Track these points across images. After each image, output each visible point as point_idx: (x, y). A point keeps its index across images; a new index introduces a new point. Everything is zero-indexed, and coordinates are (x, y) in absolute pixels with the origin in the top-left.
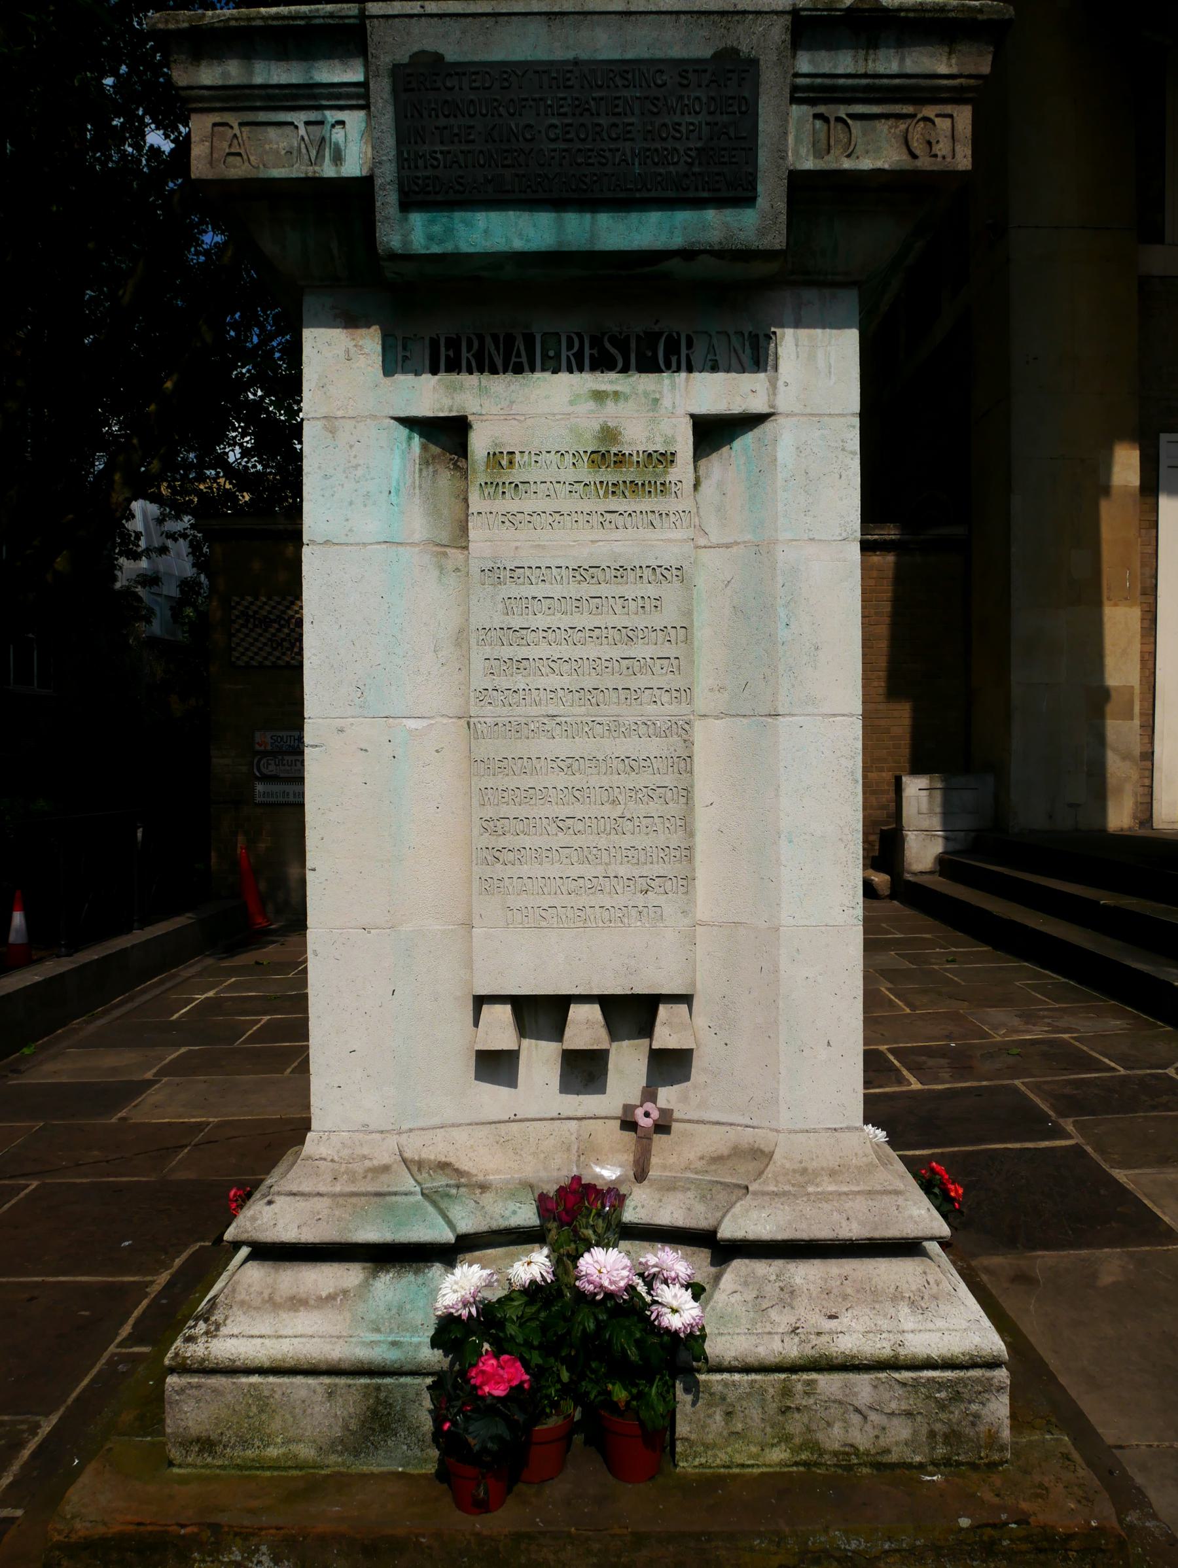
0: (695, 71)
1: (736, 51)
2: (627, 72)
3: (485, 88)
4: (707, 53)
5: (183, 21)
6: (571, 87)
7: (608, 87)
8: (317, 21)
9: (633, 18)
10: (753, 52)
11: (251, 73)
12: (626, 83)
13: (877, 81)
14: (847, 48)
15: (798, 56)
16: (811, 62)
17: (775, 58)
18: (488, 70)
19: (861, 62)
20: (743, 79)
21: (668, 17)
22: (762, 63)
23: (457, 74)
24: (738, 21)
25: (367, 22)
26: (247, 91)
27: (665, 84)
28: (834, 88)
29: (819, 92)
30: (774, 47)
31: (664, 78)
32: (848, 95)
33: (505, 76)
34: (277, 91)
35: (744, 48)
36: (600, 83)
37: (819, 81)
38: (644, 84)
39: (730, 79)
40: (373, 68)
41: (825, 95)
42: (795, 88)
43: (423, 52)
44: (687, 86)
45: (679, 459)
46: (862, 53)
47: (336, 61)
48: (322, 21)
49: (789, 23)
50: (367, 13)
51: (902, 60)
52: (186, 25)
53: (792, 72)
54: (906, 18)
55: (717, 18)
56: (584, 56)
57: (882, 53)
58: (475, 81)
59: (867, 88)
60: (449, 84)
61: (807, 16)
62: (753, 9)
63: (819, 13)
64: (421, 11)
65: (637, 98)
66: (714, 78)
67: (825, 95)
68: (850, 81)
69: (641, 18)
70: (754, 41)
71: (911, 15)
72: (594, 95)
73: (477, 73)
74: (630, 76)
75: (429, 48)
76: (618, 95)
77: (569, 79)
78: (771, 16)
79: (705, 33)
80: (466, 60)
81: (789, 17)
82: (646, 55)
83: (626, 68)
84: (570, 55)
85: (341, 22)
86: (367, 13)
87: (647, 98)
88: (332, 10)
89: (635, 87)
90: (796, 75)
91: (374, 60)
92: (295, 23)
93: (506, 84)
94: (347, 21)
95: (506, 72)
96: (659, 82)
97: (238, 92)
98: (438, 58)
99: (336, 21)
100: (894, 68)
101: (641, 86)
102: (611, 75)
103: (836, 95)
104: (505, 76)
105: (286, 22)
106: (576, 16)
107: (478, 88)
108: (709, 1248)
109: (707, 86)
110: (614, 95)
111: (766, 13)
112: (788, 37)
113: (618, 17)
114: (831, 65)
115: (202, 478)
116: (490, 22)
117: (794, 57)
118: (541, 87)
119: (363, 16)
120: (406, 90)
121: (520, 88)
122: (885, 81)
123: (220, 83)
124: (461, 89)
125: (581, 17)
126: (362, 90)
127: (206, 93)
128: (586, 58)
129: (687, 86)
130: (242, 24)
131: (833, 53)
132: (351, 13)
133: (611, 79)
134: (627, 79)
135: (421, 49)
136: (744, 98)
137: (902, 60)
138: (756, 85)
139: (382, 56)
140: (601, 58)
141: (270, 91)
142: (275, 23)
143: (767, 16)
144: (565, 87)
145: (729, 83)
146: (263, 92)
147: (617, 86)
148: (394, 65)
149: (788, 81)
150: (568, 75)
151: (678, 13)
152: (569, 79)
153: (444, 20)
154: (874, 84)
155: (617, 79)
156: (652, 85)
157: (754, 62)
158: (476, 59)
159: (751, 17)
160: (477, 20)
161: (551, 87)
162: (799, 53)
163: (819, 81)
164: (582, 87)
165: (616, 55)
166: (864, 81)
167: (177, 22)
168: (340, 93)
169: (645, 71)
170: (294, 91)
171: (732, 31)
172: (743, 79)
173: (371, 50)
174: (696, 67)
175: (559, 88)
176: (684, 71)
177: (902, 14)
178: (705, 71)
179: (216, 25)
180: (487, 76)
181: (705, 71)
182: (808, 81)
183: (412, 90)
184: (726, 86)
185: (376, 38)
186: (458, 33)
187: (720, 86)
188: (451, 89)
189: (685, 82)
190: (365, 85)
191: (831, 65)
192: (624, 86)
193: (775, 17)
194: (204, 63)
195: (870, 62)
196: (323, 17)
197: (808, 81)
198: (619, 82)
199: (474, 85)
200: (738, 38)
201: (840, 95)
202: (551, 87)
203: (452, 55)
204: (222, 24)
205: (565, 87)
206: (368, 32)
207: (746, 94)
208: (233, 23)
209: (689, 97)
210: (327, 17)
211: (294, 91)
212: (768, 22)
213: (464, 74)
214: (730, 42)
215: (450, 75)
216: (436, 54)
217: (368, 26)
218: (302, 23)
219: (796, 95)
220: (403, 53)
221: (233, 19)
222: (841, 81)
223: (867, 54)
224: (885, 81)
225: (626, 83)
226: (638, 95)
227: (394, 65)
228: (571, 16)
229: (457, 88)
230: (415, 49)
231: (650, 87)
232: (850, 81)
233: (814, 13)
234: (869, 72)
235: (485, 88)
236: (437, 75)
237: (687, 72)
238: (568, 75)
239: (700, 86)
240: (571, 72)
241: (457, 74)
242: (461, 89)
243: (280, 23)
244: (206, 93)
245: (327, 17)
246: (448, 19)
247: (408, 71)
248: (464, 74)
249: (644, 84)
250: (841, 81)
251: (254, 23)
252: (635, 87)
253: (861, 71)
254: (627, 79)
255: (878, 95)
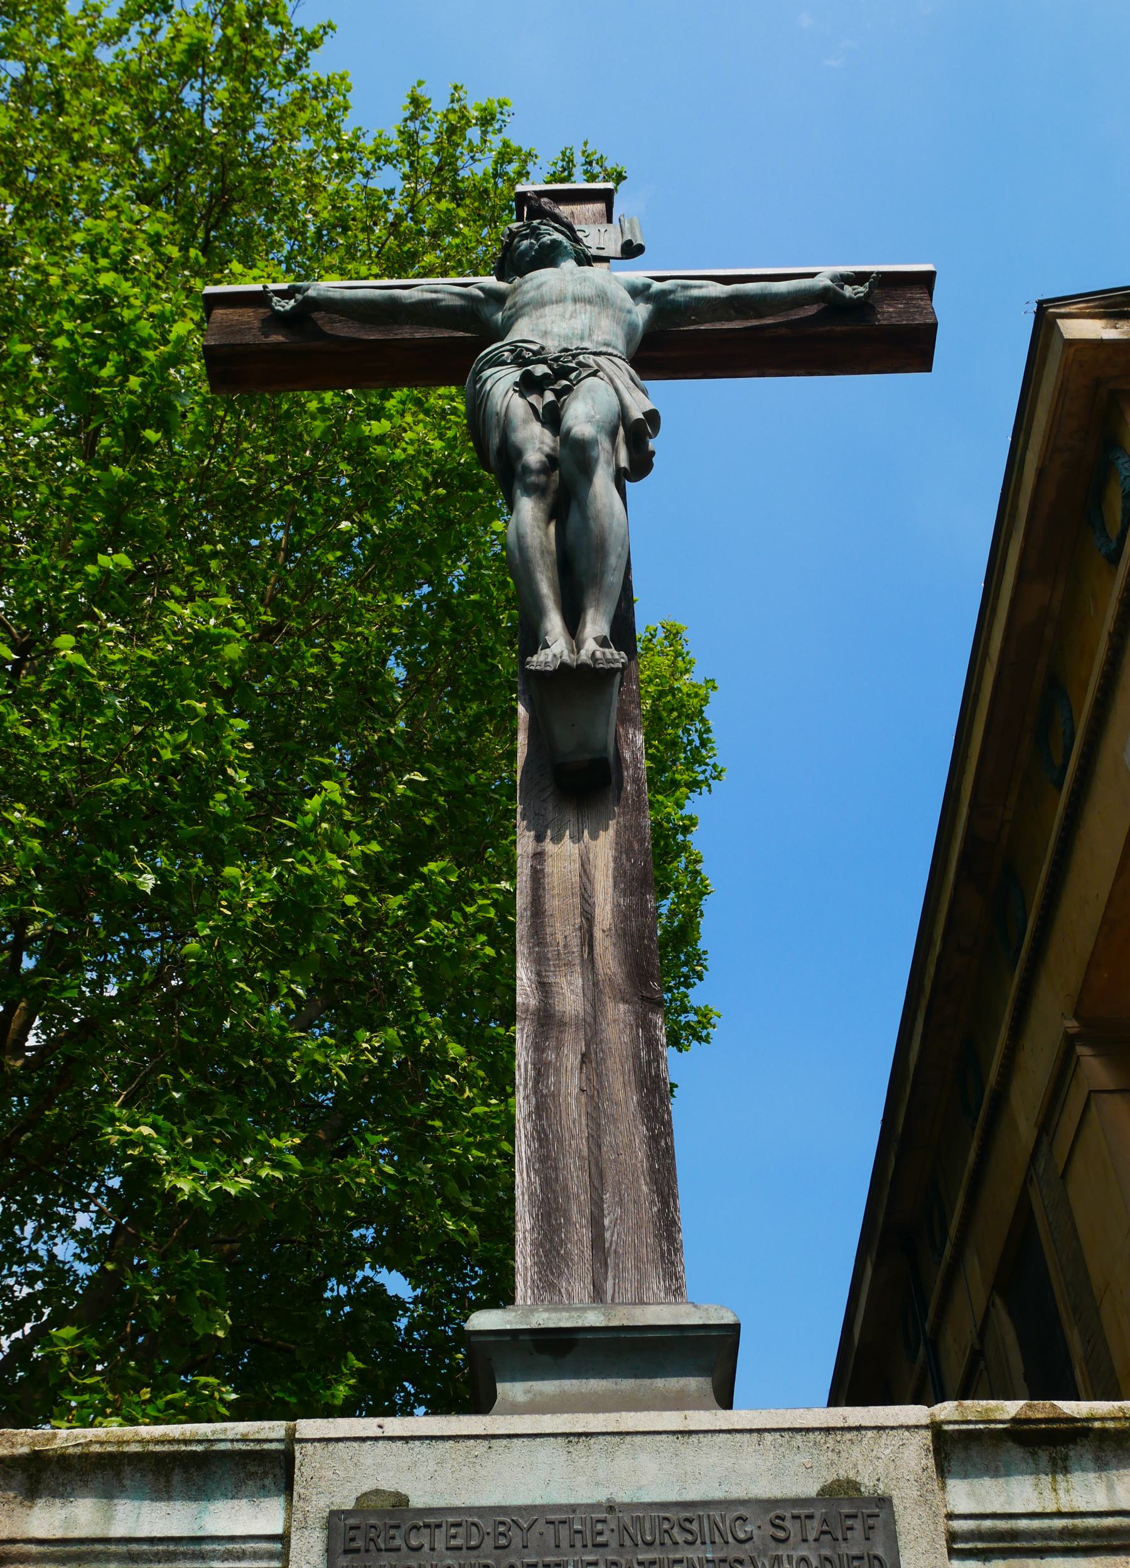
0: (795, 1517)
1: (855, 1486)
2: (690, 1521)
3: (470, 1548)
4: (810, 1488)
5: (22, 1445)
6: (605, 1545)
7: (662, 1544)
8: (221, 1446)
9: (694, 1439)
10: (881, 1486)
11: (109, 1519)
12: (690, 1538)
13: (1079, 1522)
14: (1022, 1473)
15: (949, 1488)
16: (972, 1494)
17: (916, 1493)
18: (476, 1520)
19: (1048, 1493)
20: (871, 1528)
21: (746, 1437)
22: (895, 1501)
23: (427, 1526)
24: (851, 1440)
25: (297, 1447)
26: (99, 1547)
27: (751, 1538)
28: (1014, 1535)
29: (989, 1541)
30: (912, 1477)
31: (748, 1529)
32: (1038, 1544)
33: (502, 1529)
34: (145, 1547)
35: (867, 1482)
36: (649, 1538)
37: (988, 1524)
38: (718, 1539)
39: (851, 1528)
40: (298, 1516)
41: (1001, 1545)
42: (953, 1537)
43: (377, 1492)
44: (784, 1541)
45: (722, 1413)
46: (1046, 1480)
47: (244, 1501)
48: (227, 1446)
49: (929, 1442)
50: (297, 1436)
51: (1110, 1488)
52: (25, 1450)
53: (944, 1511)
54: (1104, 1431)
55: (819, 1437)
56: (623, 1496)
57: (1077, 1478)
58: (454, 1537)
59: (1064, 1533)
60: (414, 1543)
61: (953, 1431)
62: (873, 1424)
63: (971, 1427)
64: (378, 1433)
65: (708, 1561)
66: (825, 1528)
67: (1001, 1545)
68: (1036, 1524)
69: (706, 1439)
70: (880, 1470)
71: (1110, 1425)
72: (640, 1557)
73: (457, 1525)
74: (694, 1527)
75: (385, 1486)
76: (678, 1556)
77: (600, 1533)
78: (900, 1432)
79: (804, 1458)
80: (442, 1503)
81: (928, 1434)
82: (717, 1494)
83: (688, 1515)
84: (600, 1496)
85: (258, 1447)
86: (297, 1436)
87: (723, 1561)
88: (245, 1431)
89: (703, 1543)
90: (950, 1516)
91: (301, 1504)
92: (189, 1448)
93: (503, 1541)
94: (266, 1446)
95: (503, 1523)
96: (742, 1536)
97: (84, 1548)
98: (400, 1501)
99: (251, 1446)
100: (1101, 1503)
101: (713, 1543)
102: (666, 1526)
103: (1018, 1545)
104: (502, 1529)
105: (175, 1448)
106: (608, 1438)
107: (459, 1548)
108: (708, 1376)
109: (816, 1540)
110: (671, 1556)
111: (892, 1428)
112: (931, 1462)
113: (671, 1438)
114: (1002, 1499)
115: (48, 799)
116: (481, 1446)
117: (943, 1488)
118: (558, 1546)
119: (291, 1439)
120: (347, 1552)
121: (525, 1547)
122: (1092, 1522)
123: (59, 1534)
124: (432, 1549)
125: (617, 1439)
126: (278, 1546)
127: (34, 1549)
128: (626, 1500)
129: (784, 1541)
130: (109, 1449)
131: (1001, 1480)
132: (273, 1436)
133: (666, 1531)
134: (690, 1532)
135: (374, 1487)
136: (876, 1557)
137: (1110, 1488)
138: (892, 1538)
139: (314, 1498)
140: (647, 1499)
141: (134, 1547)
142: (158, 1448)
143: (894, 1432)
144: (594, 1546)
145: (849, 1534)
146: (122, 1549)
147: (676, 1543)
148: (332, 1513)
149: (942, 1528)
150: (599, 1527)
151: (759, 1431)
152: (600, 1533)
153: (411, 1444)
154: (1075, 1527)
155: (676, 1531)
156: (731, 1539)
157: (884, 1502)
158: (457, 1502)
159: (870, 1434)
160: (462, 1444)
161: (572, 1546)
162: (951, 1483)
163: (988, 1524)
164: (622, 1545)
165: (673, 1496)
166: (1058, 1523)
167: (13, 1445)
168: (244, 1552)
169: (718, 1519)
170: (172, 1548)
171: (843, 1454)
172: (871, 1528)
173: (297, 1488)
174: (796, 1512)
175: (585, 1546)
176: (778, 1517)
177: (1097, 1425)
178: (810, 1517)
179: (70, 1451)
180: (474, 1529)
181: (810, 1517)
182: (970, 1524)
183: (357, 1551)
184: (845, 1539)
185: (307, 1471)
186: (431, 1463)
187: (836, 1540)
188: (418, 1549)
189: (781, 1534)
190: (283, 1539)
191: (1002, 1499)
192: (687, 1542)
193: (906, 1433)
194: (40, 1502)
195: (1061, 1493)
196: (232, 1441)
197: (970, 1524)
198: (679, 1537)
199: (453, 1542)
200: (855, 1465)
201: (1025, 1544)
202: (572, 1546)
203: (418, 1501)
204: (78, 1450)
205: (594, 1546)
206: (297, 1462)
207: (880, 1552)
208: (96, 1448)
209: (790, 1558)
210: (238, 1441)
211: (172, 1548)
212: (897, 1442)
213: (439, 1526)
214: (844, 1471)
215: (416, 1527)
216: (397, 1494)
217: (297, 1454)
218: (199, 1448)
219: (955, 1546)
220: (346, 1493)
221: (97, 1442)
222: (1023, 1524)
223: (1054, 1480)
224: (1092, 1522)
225: (690, 1538)
226: (709, 1556)
227: (332, 1513)
228: (601, 1438)
229: (427, 1547)
230: (366, 1488)
231: (727, 1543)
232: (1036, 1524)
233: (964, 1427)
234: (1064, 1510)
235: (470, 1548)
236: (397, 1527)
237: (783, 1519)
238: (599, 1527)
239: (805, 1540)
240: (604, 1521)
241: (427, 1526)
242: (432, 1549)
243: (166, 1448)
244: (34, 1549)
245: (238, 1441)
246: (417, 1443)
247: (352, 1521)
248: (439, 1526)
249: (718, 1539)
250: (1023, 1524)
251: (126, 1449)
252: (703, 1543)
253: (1051, 1508)
254: (690, 1532)
255: (1083, 1543)
